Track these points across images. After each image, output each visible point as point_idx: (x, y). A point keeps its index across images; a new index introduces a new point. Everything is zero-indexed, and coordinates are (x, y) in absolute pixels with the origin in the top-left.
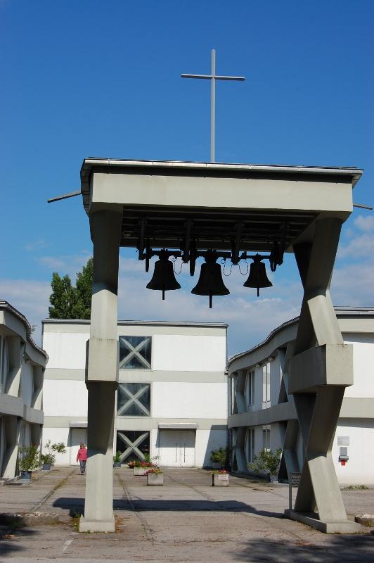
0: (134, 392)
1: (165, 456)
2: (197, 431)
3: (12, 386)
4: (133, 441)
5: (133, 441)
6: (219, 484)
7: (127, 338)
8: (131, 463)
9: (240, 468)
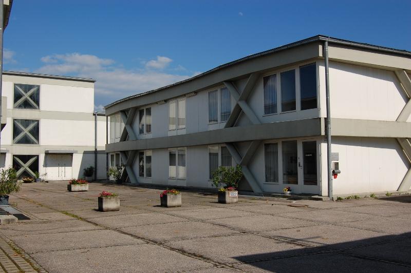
0: (26, 126)
1: (51, 173)
2: (74, 155)
3: (241, 75)
4: (25, 163)
5: (25, 163)
6: (230, 201)
7: (21, 86)
8: (26, 179)
9: (132, 181)
